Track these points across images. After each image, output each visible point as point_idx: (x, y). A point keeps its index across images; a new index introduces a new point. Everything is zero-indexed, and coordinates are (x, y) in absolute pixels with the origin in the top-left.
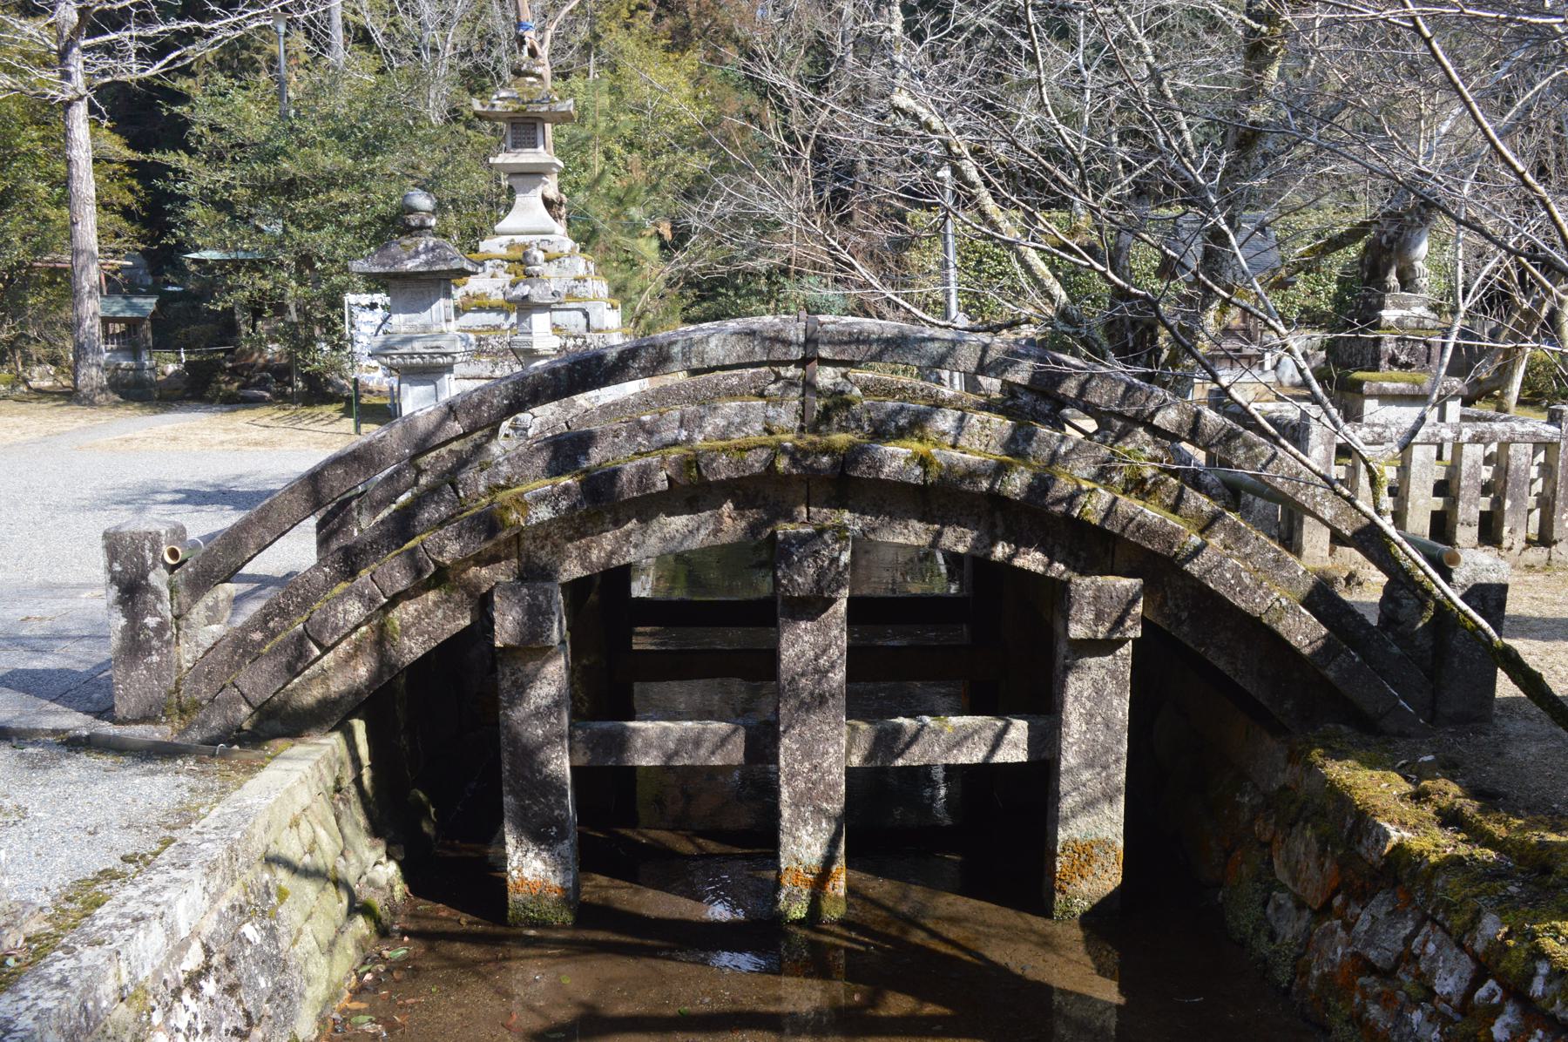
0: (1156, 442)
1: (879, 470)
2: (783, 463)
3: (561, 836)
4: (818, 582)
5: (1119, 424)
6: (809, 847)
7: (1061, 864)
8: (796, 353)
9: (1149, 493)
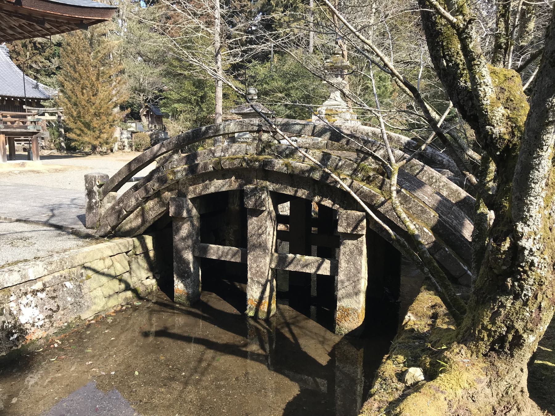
0: (376, 162)
1: (273, 167)
2: (244, 164)
3: (188, 277)
4: (255, 204)
5: (363, 155)
6: (256, 292)
7: (338, 314)
8: (256, 128)
9: (371, 181)
